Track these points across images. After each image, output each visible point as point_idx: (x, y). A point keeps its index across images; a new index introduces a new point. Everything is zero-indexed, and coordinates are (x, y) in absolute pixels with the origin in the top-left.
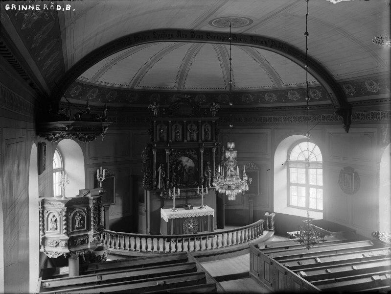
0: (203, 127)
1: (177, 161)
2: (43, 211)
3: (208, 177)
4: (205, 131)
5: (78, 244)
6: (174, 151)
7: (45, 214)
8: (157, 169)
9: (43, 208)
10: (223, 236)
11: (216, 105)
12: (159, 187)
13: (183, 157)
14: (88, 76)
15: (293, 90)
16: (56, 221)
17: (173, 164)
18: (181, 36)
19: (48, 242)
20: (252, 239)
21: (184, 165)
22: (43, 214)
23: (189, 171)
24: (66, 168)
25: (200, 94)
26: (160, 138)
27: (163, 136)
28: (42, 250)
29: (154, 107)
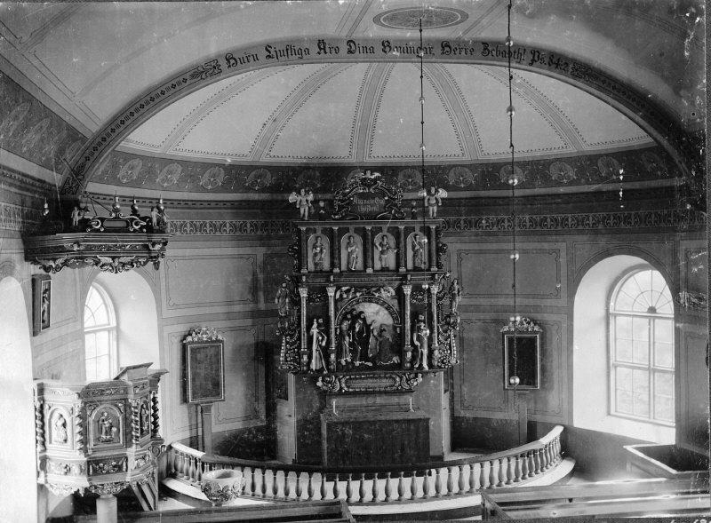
0: (409, 240)
1: (354, 313)
2: (42, 406)
3: (422, 346)
4: (414, 247)
5: (108, 472)
6: (348, 292)
7: (45, 412)
8: (309, 327)
9: (42, 399)
10: (450, 471)
11: (437, 191)
12: (313, 366)
13: (366, 305)
14: (148, 137)
15: (607, 155)
16: (64, 425)
17: (345, 318)
18: (328, 50)
19: (51, 465)
20: (516, 481)
21: (369, 322)
22: (41, 412)
23: (380, 335)
24: (123, 327)
25: (407, 167)
26: (316, 264)
27: (321, 259)
28: (42, 480)
29: (302, 200)
